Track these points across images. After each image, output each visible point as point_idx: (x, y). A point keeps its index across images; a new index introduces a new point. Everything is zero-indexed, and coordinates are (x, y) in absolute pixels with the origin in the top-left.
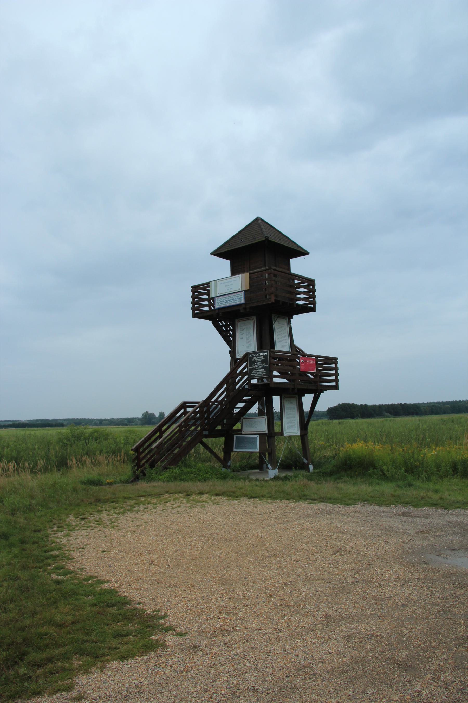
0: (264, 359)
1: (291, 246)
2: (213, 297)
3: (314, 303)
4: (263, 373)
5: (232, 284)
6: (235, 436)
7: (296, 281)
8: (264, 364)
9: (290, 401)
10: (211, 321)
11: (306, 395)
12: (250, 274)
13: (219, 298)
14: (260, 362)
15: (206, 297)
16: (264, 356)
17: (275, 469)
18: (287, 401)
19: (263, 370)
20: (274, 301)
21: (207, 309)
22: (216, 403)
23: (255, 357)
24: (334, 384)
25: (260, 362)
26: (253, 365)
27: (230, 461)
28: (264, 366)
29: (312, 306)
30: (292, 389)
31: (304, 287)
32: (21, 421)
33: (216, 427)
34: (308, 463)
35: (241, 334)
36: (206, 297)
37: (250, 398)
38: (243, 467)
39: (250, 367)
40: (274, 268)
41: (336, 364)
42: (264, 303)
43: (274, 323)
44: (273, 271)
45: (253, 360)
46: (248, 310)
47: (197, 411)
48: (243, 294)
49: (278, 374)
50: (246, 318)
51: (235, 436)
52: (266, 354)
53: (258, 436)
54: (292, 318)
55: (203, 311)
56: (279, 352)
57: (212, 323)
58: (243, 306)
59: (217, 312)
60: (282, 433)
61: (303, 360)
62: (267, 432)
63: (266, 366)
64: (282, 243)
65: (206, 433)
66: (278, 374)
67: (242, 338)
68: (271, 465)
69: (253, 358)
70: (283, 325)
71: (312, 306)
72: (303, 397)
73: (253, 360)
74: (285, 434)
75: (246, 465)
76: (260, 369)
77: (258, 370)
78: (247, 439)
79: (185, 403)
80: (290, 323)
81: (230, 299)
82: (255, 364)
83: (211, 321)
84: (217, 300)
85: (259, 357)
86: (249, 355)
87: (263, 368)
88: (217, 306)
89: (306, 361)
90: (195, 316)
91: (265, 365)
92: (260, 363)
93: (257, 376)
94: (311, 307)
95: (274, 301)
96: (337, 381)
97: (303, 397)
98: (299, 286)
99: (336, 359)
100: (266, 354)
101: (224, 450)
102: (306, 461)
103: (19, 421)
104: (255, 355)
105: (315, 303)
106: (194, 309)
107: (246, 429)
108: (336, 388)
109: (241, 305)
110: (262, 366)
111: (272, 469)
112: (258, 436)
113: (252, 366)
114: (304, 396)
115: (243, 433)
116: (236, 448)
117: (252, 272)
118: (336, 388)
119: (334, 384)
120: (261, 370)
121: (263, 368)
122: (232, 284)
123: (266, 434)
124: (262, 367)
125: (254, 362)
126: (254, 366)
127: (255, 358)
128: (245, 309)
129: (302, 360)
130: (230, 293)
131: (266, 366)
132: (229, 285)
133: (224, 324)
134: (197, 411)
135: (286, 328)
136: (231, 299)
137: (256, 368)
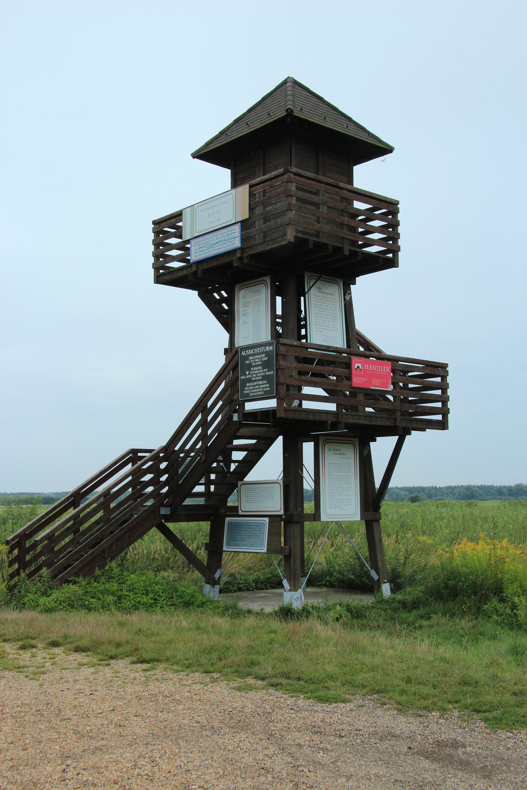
0: (266, 359)
1: (351, 132)
2: (187, 239)
3: (395, 250)
4: (265, 389)
5: (220, 211)
6: (227, 519)
7: (359, 205)
8: (266, 370)
9: (340, 450)
10: (196, 293)
11: (378, 438)
12: (250, 187)
13: (197, 240)
14: (259, 365)
15: (174, 241)
16: (267, 354)
17: (295, 590)
18: (330, 450)
19: (265, 382)
20: (292, 240)
21: (176, 265)
22: (192, 454)
23: (252, 355)
24: (439, 417)
25: (259, 365)
26: (247, 373)
27: (219, 570)
28: (267, 373)
29: (391, 255)
30: (332, 423)
31: (381, 217)
32: (43, 493)
33: (183, 501)
34: (379, 579)
35: (244, 315)
36: (174, 241)
37: (254, 441)
38: (262, 583)
39: (242, 378)
40: (294, 170)
41: (444, 378)
42: (276, 246)
43: (309, 290)
44: (292, 175)
45: (247, 362)
46: (246, 261)
47: (145, 467)
48: (237, 228)
49: (325, 394)
50: (253, 281)
51: (227, 519)
52: (271, 348)
53: (267, 519)
54: (354, 283)
55: (172, 270)
56: (319, 347)
57: (199, 295)
58: (238, 255)
59: (194, 268)
60: (316, 516)
61: (360, 365)
62: (282, 513)
63: (270, 373)
64: (329, 124)
65: (164, 511)
66: (325, 394)
67: (245, 323)
68: (289, 581)
69: (248, 356)
70: (329, 296)
71: (391, 255)
72: (372, 444)
73: (247, 362)
74: (324, 518)
75: (268, 579)
76: (259, 380)
77: (255, 383)
78: (247, 525)
79: (134, 452)
80: (347, 290)
81: (216, 241)
82: (250, 370)
83: (196, 293)
84: (192, 246)
85: (257, 357)
86: (241, 353)
87: (264, 378)
88: (194, 257)
89: (366, 366)
90: (159, 279)
91: (268, 371)
92: (260, 368)
93: (254, 396)
94: (389, 259)
95: (292, 240)
96: (445, 412)
97: (372, 444)
98: (370, 215)
99: (444, 366)
100: (271, 348)
101: (207, 546)
102: (375, 576)
103: (38, 494)
104: (251, 352)
105: (398, 249)
106: (156, 268)
107: (246, 507)
108: (443, 425)
109: (233, 252)
110: (263, 374)
111: (290, 590)
112: (267, 519)
113: (246, 375)
114: (375, 440)
115: (240, 513)
116: (228, 544)
117: (254, 182)
118: (443, 425)
119: (439, 417)
120: (261, 383)
121: (264, 378)
122: (220, 211)
123: (280, 516)
124: (263, 376)
125: (250, 366)
126: (249, 374)
127: (251, 358)
128: (241, 259)
129: (357, 365)
130: (216, 228)
131: (270, 373)
132: (214, 214)
133: (215, 294)
134: (145, 467)
135: (337, 301)
136: (217, 241)
137: (253, 379)
